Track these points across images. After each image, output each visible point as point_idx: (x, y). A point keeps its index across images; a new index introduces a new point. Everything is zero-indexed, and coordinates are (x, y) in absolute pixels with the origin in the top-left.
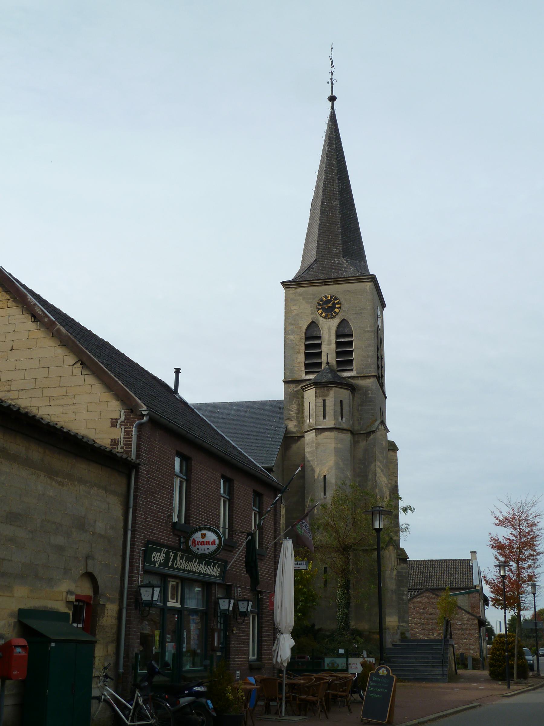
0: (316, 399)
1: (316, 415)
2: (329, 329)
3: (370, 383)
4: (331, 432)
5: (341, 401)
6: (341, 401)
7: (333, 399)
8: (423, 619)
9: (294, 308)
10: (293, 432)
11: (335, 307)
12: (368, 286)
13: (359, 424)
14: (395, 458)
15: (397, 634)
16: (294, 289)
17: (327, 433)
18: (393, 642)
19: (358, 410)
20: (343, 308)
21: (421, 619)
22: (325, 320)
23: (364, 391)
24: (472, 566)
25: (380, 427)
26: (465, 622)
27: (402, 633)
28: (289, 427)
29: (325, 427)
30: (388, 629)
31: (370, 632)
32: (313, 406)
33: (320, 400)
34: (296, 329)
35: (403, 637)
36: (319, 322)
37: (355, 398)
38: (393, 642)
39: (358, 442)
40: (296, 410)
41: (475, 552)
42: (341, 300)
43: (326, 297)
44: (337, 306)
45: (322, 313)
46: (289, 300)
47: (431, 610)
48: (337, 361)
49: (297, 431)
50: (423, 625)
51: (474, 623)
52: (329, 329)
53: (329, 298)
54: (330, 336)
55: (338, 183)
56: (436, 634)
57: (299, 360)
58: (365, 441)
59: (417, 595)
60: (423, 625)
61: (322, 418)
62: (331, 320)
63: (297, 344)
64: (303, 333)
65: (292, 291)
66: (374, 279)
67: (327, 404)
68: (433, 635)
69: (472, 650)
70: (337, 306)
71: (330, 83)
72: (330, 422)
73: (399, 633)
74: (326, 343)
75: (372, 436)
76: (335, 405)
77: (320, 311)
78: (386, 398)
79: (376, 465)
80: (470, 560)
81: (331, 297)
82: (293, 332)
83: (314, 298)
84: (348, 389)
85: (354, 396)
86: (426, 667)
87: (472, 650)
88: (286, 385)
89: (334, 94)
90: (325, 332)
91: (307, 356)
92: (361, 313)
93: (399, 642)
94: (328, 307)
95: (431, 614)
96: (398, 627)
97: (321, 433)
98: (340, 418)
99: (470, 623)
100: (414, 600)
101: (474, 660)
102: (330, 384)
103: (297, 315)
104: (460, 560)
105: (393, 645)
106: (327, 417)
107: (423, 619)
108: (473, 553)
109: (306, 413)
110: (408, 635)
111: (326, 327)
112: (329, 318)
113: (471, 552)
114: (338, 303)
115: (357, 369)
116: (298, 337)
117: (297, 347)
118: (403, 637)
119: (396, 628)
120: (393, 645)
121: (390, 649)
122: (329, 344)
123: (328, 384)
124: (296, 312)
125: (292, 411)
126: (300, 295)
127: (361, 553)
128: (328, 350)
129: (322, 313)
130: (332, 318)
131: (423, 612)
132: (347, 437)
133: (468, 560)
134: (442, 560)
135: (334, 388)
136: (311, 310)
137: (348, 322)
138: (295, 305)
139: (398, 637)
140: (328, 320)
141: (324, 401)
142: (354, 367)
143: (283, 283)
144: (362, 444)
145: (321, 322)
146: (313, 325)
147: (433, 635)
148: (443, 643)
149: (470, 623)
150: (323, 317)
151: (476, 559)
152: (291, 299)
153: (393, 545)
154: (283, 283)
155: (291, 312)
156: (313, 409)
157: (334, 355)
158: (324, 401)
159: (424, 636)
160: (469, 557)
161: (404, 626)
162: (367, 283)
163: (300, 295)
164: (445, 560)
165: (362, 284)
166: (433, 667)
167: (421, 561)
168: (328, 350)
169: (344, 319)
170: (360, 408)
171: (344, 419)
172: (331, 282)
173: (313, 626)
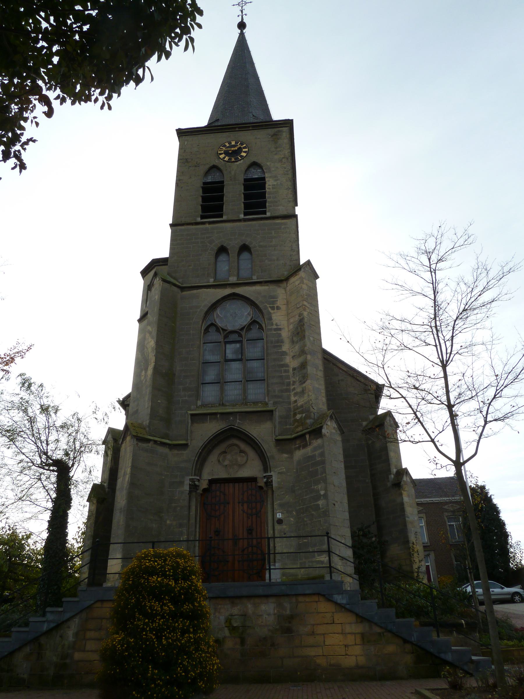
11: (241, 151)
44: (244, 150)
45: (224, 158)
65: (189, 138)
70: (244, 150)
71: (240, 17)
81: (236, 143)
129: (224, 158)
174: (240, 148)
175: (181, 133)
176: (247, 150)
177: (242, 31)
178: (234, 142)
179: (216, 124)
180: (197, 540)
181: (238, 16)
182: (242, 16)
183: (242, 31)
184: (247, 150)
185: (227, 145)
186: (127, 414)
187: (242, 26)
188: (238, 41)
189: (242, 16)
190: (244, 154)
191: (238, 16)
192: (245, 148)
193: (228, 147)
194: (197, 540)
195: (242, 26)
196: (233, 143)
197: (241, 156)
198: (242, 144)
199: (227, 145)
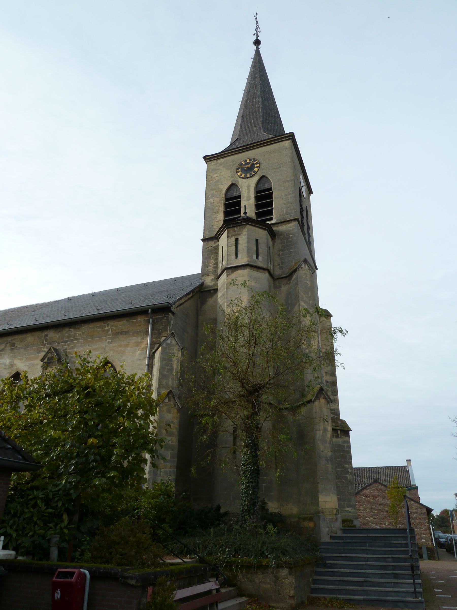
0: (228, 240)
1: (227, 255)
2: (248, 187)
3: (293, 227)
4: (244, 269)
5: (257, 240)
6: (257, 240)
7: (247, 236)
8: (374, 509)
9: (215, 176)
10: (209, 286)
11: (254, 167)
12: (287, 144)
13: (281, 268)
14: (328, 324)
15: (336, 520)
16: (215, 161)
17: (239, 272)
18: (332, 532)
19: (279, 255)
20: (262, 166)
21: (372, 508)
22: (244, 180)
23: (286, 236)
24: (409, 471)
25: (303, 266)
26: (414, 511)
27: (344, 521)
28: (206, 282)
29: (238, 265)
30: (323, 512)
31: (299, 518)
32: (225, 248)
33: (233, 240)
34: (216, 193)
35: (348, 525)
36: (238, 183)
37: (276, 244)
38: (332, 532)
39: (280, 287)
40: (214, 264)
41: (410, 460)
42: (260, 161)
43: (245, 161)
44: (256, 166)
45: (241, 175)
46: (211, 171)
47: (381, 500)
48: (256, 213)
49: (214, 285)
50: (375, 514)
51: (423, 512)
52: (248, 187)
53: (248, 161)
54: (249, 192)
55: (260, 87)
56: (387, 523)
57: (218, 219)
58: (287, 285)
59: (367, 486)
60: (375, 514)
61: (234, 256)
62: (251, 178)
63: (217, 205)
64: (223, 195)
65: (214, 163)
66: (291, 136)
67: (240, 242)
68: (385, 524)
69: (424, 538)
70: (256, 166)
71: (256, 34)
72: (243, 259)
73: (340, 520)
74: (245, 199)
75: (295, 276)
76: (248, 242)
77: (239, 174)
78: (317, 269)
79: (299, 305)
80: (406, 466)
81: (250, 160)
82: (213, 196)
83: (234, 165)
84: (265, 229)
85: (274, 242)
86: (383, 576)
87: (424, 538)
88: (205, 243)
89: (259, 38)
90: (244, 190)
91: (227, 214)
92: (280, 167)
93: (340, 533)
94: (248, 169)
95: (381, 504)
96: (338, 511)
97: (232, 272)
98: (255, 257)
99: (419, 512)
100: (365, 491)
101: (428, 549)
102: (244, 222)
103: (218, 181)
104: (399, 467)
105: (332, 537)
106: (239, 256)
107: (374, 509)
108: (408, 461)
109: (220, 259)
110: (357, 523)
111: (245, 185)
112: (248, 178)
113: (407, 460)
114: (257, 163)
115: (276, 217)
116: (218, 199)
117: (217, 208)
118: (348, 525)
119: (335, 512)
120: (332, 537)
121: (328, 543)
122: (248, 199)
123: (241, 223)
124: (217, 179)
125: (209, 266)
126: (221, 164)
127: (286, 413)
128: (248, 205)
129: (241, 175)
130: (251, 177)
131: (374, 502)
132: (265, 276)
133: (405, 467)
134: (385, 467)
135: (248, 226)
136: (231, 175)
137: (267, 178)
138: (216, 173)
139: (338, 525)
140: (247, 180)
141: (237, 240)
142: (274, 216)
143: (205, 158)
144: (285, 289)
145: (240, 183)
146: (233, 186)
147: (385, 524)
148: (409, 535)
149: (419, 512)
150: (242, 178)
151: (411, 465)
152: (213, 170)
153: (325, 398)
154: (205, 158)
155: (212, 180)
156: (225, 251)
157: (254, 208)
158: (237, 240)
159: (377, 525)
160: (405, 464)
161: (350, 512)
162: (285, 142)
163: (221, 164)
164: (387, 467)
165: (281, 143)
166: (396, 576)
167: (370, 468)
168: (248, 205)
169: (263, 176)
170: (281, 253)
171: (260, 258)
172: (250, 147)
173: (219, 508)
174: (254, 164)
175: (207, 159)
176: (258, 165)
177: (257, 48)
178: (249, 160)
179: (234, 147)
180: (414, 581)
181: (254, 35)
182: (257, 34)
183: (257, 48)
184: (258, 165)
185: (244, 163)
186: (336, 412)
187: (257, 42)
188: (255, 59)
189: (257, 34)
190: (256, 169)
191: (254, 35)
192: (257, 164)
193: (244, 165)
194: (414, 581)
195: (257, 42)
196: (248, 161)
197: (254, 172)
198: (254, 161)
199: (244, 163)
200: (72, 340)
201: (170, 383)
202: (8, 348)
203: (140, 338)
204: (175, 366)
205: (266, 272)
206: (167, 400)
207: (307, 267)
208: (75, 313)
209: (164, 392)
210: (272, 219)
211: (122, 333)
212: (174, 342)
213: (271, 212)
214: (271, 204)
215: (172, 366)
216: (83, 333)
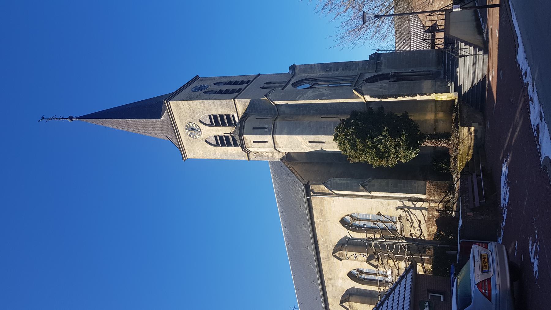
5: (254, 128)
6: (254, 128)
61: (266, 143)
77: (198, 137)
81: (186, 129)
91: (229, 145)
97: (277, 144)
114: (189, 125)
142: (231, 114)
171: (266, 127)
190: (194, 125)
200: (326, 243)
201: (355, 184)
202: (332, 282)
203: (325, 202)
204: (344, 182)
205: (275, 122)
206: (367, 187)
207: (270, 94)
208: (206, 105)
209: (361, 188)
210: (233, 116)
211: (322, 213)
212: (329, 182)
213: (228, 116)
214: (221, 116)
215: (344, 184)
216: (322, 236)
